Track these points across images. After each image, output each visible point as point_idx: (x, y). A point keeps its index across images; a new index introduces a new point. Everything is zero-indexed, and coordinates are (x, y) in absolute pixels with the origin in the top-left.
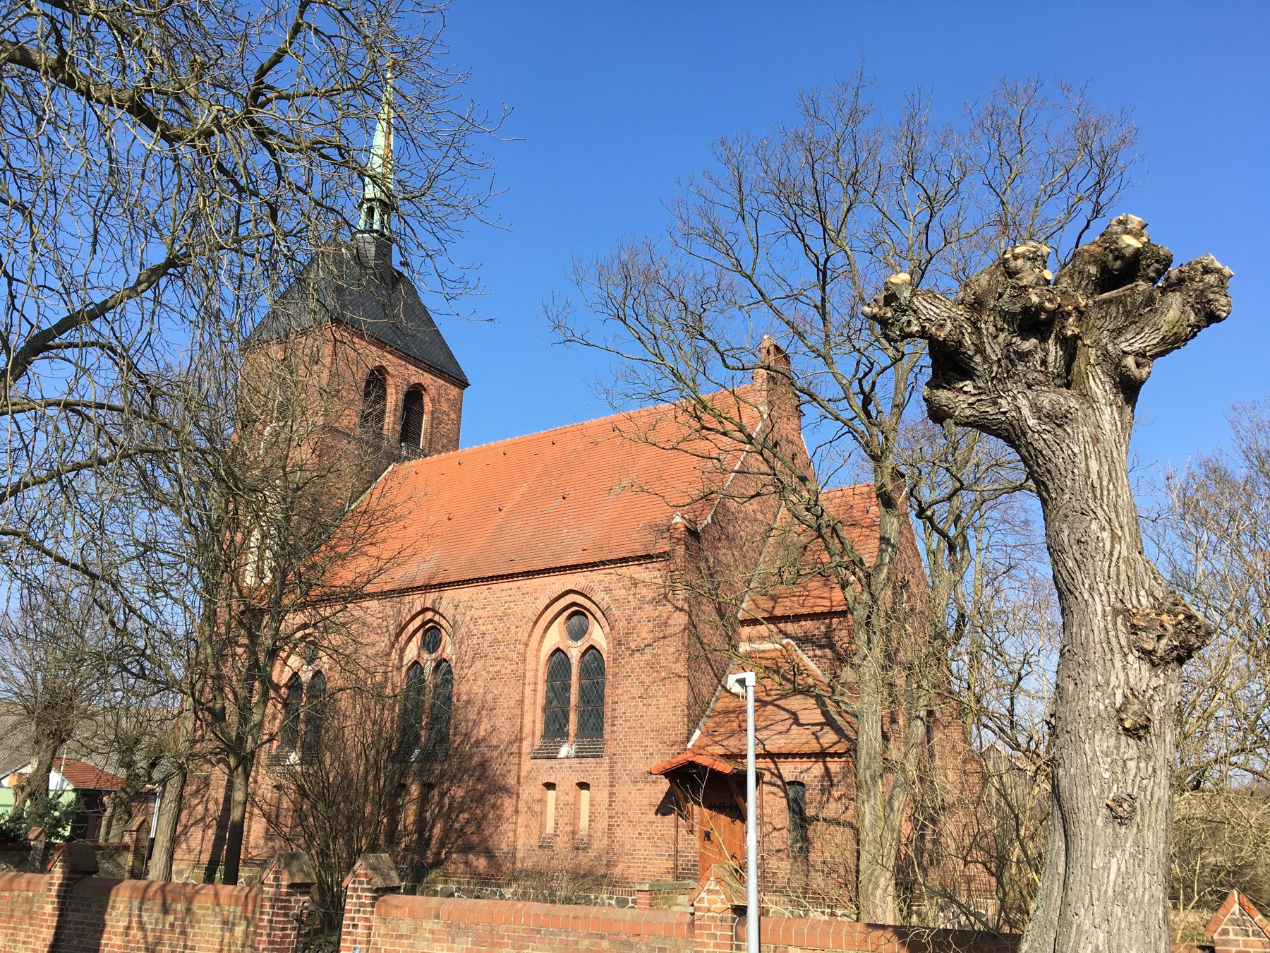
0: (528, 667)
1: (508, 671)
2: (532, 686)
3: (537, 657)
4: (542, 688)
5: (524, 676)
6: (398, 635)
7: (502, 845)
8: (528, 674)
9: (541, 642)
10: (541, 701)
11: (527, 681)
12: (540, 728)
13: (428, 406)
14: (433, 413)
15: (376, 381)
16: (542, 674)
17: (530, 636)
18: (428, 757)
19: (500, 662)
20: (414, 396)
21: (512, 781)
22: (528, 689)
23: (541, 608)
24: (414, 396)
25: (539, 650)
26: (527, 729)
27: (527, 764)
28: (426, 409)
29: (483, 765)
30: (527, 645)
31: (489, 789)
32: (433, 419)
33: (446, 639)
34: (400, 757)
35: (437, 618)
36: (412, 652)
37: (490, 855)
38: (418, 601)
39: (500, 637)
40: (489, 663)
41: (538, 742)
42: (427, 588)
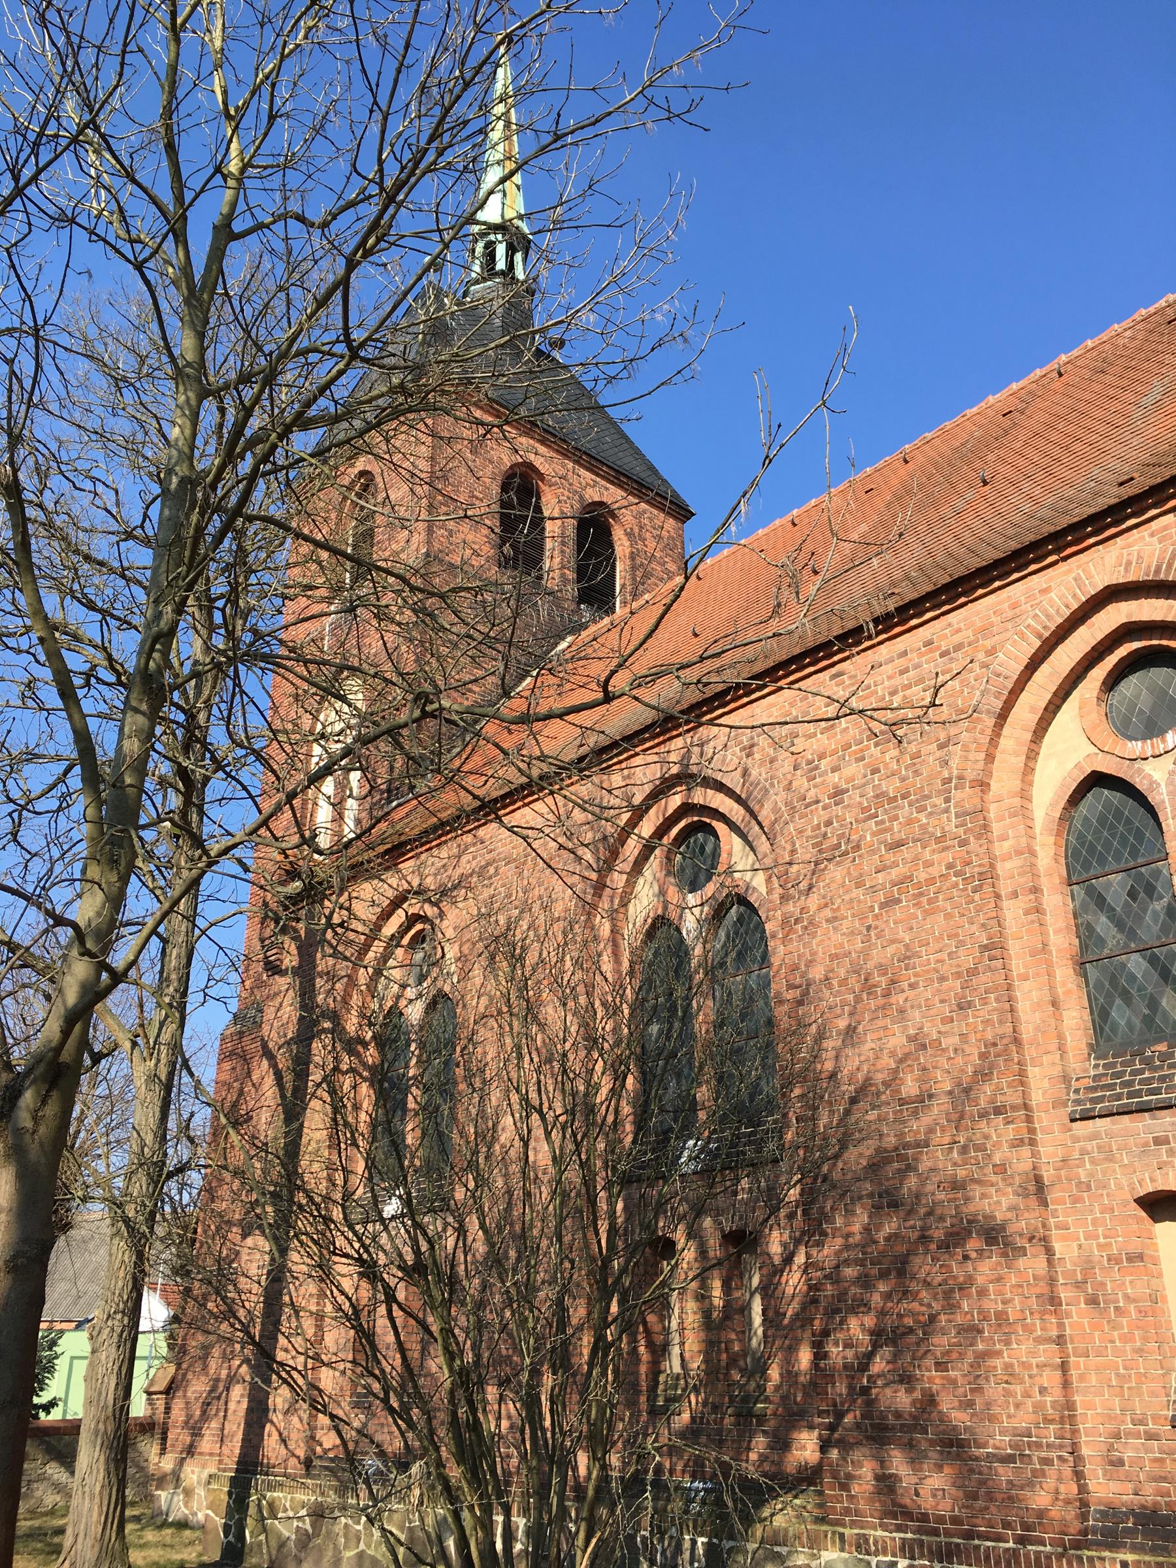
0: (1001, 848)
1: (938, 869)
2: (1024, 901)
3: (1023, 812)
4: (1058, 903)
5: (989, 875)
6: (607, 866)
7: (1007, 1406)
8: (1002, 868)
9: (1028, 770)
10: (1062, 940)
11: (1005, 888)
12: (1076, 1019)
13: (622, 546)
14: (633, 557)
15: (521, 486)
16: (1048, 856)
17: (990, 758)
18: (721, 1164)
19: (906, 853)
20: (594, 528)
21: (997, 1201)
22: (1013, 911)
23: (1016, 669)
24: (594, 528)
25: (1025, 794)
26: (1030, 1015)
27: (1055, 1139)
28: (619, 551)
29: (892, 1163)
30: (983, 785)
31: (917, 1239)
32: (634, 568)
33: (732, 846)
34: (640, 1175)
35: (701, 796)
36: (644, 902)
37: (954, 1447)
38: (643, 770)
39: (891, 787)
40: (868, 864)
41: (1082, 1065)
42: (664, 725)
